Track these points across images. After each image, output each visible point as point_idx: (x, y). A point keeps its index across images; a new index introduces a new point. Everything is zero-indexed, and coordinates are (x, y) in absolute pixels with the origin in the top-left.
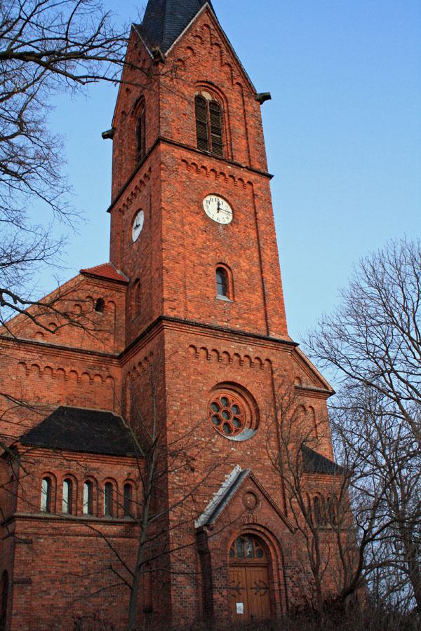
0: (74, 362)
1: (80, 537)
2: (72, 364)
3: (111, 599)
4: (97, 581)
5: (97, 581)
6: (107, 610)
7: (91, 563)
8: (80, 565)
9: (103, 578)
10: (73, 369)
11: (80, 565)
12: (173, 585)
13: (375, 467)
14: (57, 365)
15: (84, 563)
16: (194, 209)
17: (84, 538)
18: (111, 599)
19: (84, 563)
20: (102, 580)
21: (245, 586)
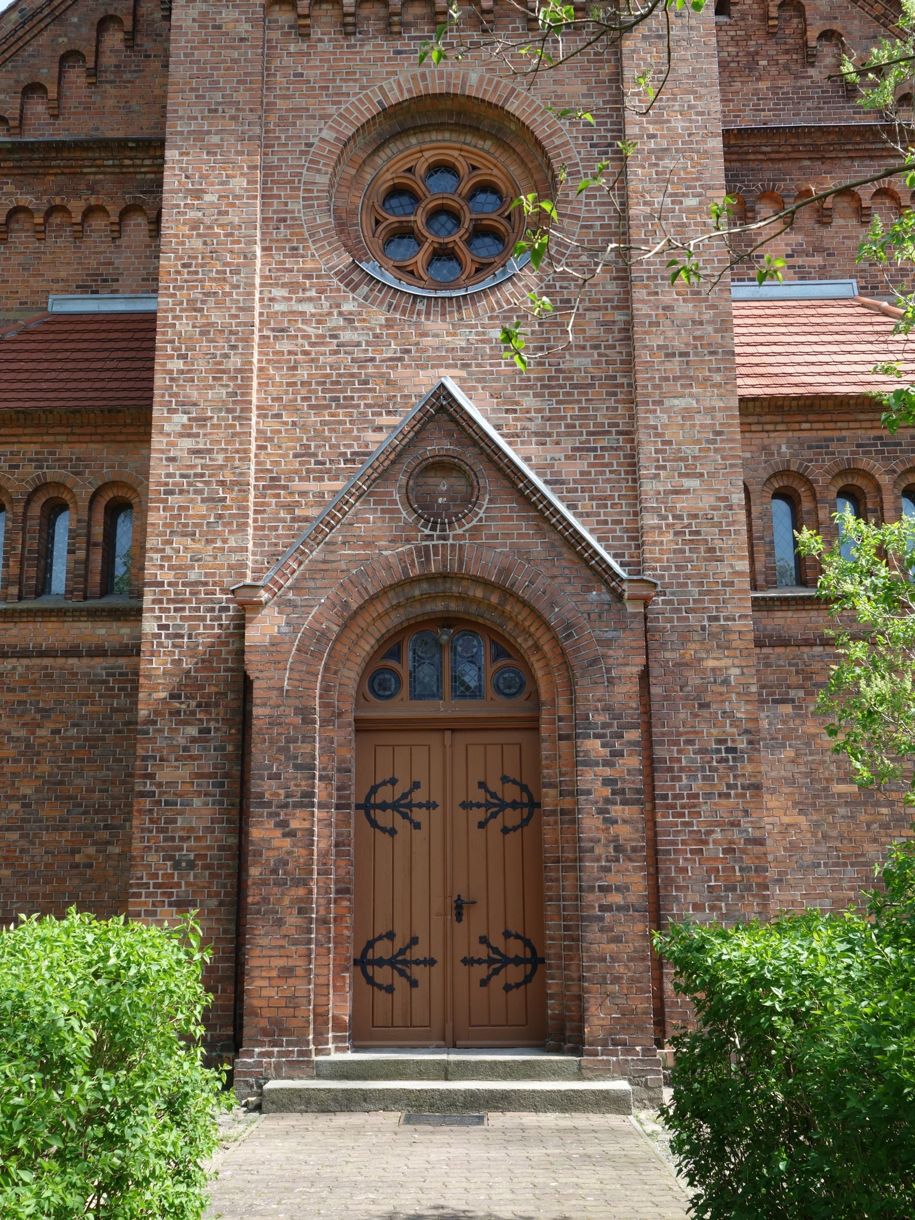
0: (96, 182)
1: (14, 660)
2: (92, 189)
3: (105, 835)
4: (61, 783)
5: (61, 783)
6: (90, 866)
7: (44, 732)
8: (11, 739)
9: (80, 774)
10: (93, 201)
11: (11, 739)
12: (142, 794)
13: (794, 680)
14: (45, 198)
15: (22, 733)
16: (526, 640)
17: (25, 662)
18: (105, 835)
19: (22, 733)
20: (78, 781)
21: (436, 797)
